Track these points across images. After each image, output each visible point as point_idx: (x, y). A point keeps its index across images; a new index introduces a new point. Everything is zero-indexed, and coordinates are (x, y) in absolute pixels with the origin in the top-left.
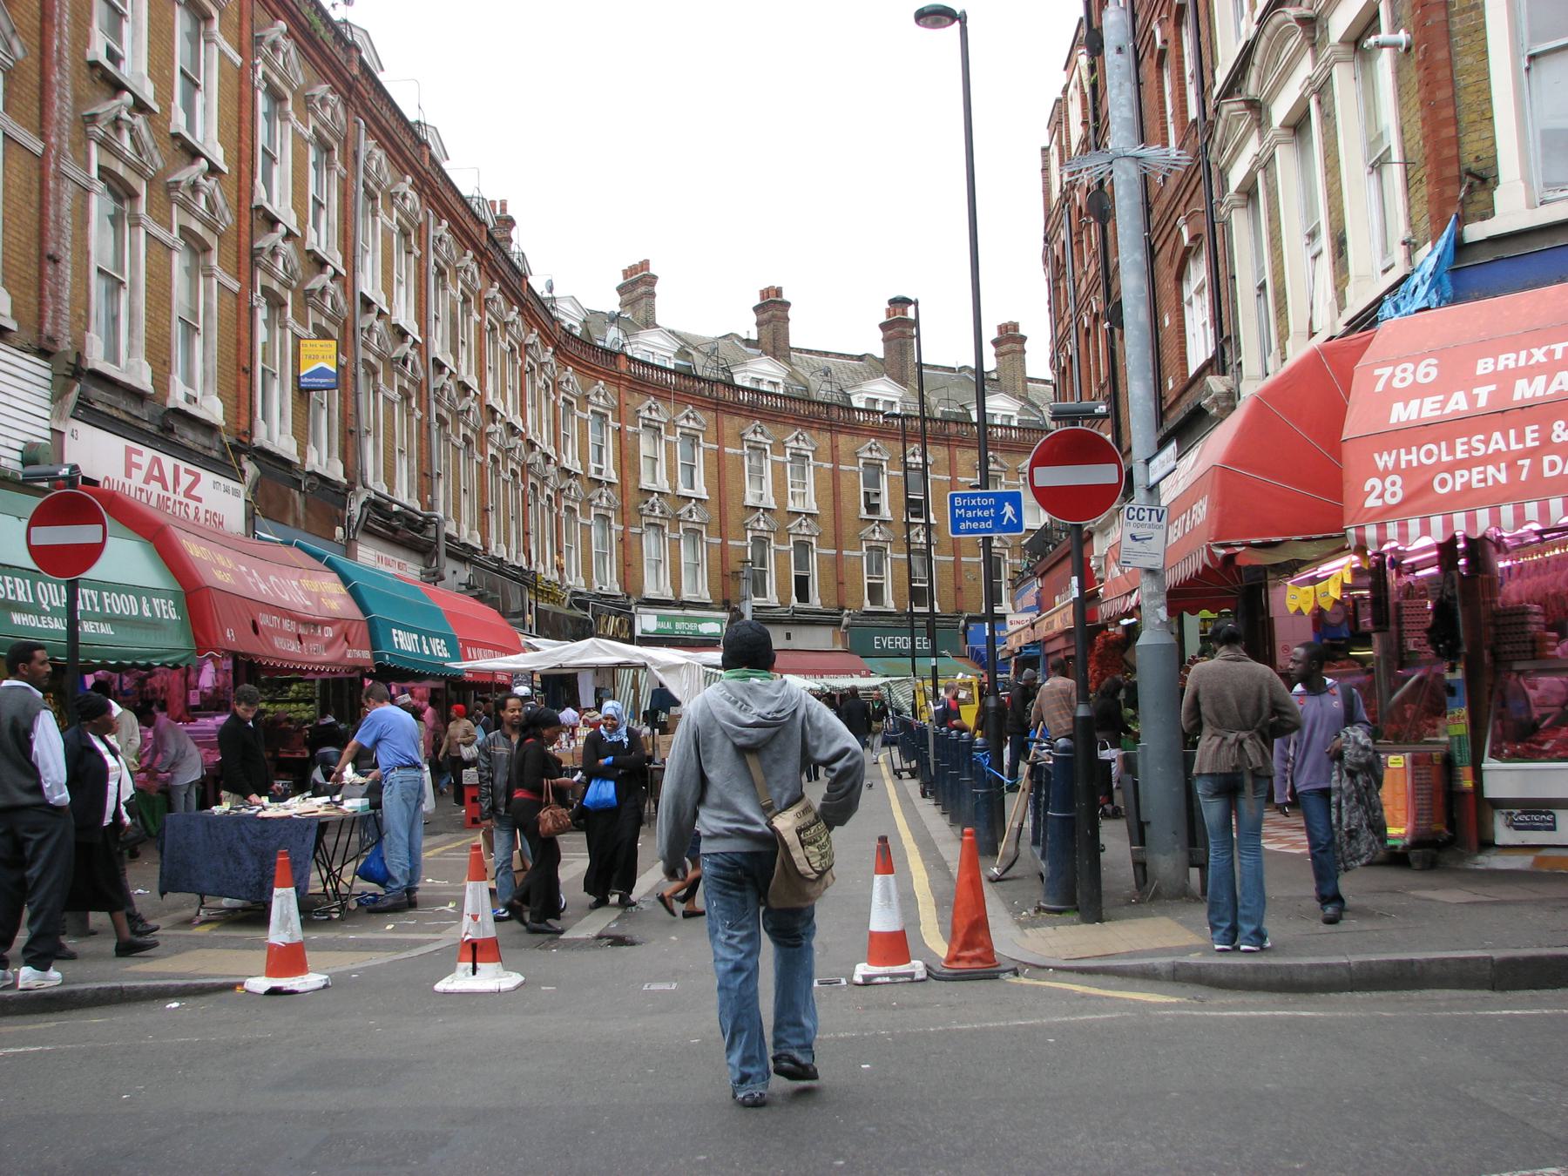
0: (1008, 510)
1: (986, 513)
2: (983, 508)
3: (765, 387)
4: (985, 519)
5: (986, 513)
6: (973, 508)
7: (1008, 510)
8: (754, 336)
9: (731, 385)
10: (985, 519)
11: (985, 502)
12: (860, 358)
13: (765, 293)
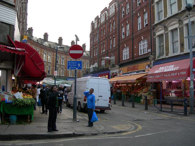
0: (79, 65)
1: (75, 65)
2: (74, 64)
3: (46, 46)
4: (74, 66)
5: (75, 65)
6: (72, 64)
7: (79, 65)
8: (43, 39)
9: (42, 44)
10: (74, 66)
11: (75, 63)
12: (55, 43)
13: (45, 33)
